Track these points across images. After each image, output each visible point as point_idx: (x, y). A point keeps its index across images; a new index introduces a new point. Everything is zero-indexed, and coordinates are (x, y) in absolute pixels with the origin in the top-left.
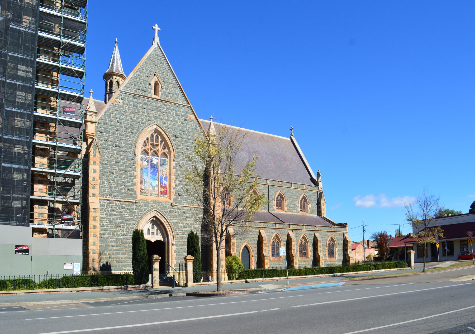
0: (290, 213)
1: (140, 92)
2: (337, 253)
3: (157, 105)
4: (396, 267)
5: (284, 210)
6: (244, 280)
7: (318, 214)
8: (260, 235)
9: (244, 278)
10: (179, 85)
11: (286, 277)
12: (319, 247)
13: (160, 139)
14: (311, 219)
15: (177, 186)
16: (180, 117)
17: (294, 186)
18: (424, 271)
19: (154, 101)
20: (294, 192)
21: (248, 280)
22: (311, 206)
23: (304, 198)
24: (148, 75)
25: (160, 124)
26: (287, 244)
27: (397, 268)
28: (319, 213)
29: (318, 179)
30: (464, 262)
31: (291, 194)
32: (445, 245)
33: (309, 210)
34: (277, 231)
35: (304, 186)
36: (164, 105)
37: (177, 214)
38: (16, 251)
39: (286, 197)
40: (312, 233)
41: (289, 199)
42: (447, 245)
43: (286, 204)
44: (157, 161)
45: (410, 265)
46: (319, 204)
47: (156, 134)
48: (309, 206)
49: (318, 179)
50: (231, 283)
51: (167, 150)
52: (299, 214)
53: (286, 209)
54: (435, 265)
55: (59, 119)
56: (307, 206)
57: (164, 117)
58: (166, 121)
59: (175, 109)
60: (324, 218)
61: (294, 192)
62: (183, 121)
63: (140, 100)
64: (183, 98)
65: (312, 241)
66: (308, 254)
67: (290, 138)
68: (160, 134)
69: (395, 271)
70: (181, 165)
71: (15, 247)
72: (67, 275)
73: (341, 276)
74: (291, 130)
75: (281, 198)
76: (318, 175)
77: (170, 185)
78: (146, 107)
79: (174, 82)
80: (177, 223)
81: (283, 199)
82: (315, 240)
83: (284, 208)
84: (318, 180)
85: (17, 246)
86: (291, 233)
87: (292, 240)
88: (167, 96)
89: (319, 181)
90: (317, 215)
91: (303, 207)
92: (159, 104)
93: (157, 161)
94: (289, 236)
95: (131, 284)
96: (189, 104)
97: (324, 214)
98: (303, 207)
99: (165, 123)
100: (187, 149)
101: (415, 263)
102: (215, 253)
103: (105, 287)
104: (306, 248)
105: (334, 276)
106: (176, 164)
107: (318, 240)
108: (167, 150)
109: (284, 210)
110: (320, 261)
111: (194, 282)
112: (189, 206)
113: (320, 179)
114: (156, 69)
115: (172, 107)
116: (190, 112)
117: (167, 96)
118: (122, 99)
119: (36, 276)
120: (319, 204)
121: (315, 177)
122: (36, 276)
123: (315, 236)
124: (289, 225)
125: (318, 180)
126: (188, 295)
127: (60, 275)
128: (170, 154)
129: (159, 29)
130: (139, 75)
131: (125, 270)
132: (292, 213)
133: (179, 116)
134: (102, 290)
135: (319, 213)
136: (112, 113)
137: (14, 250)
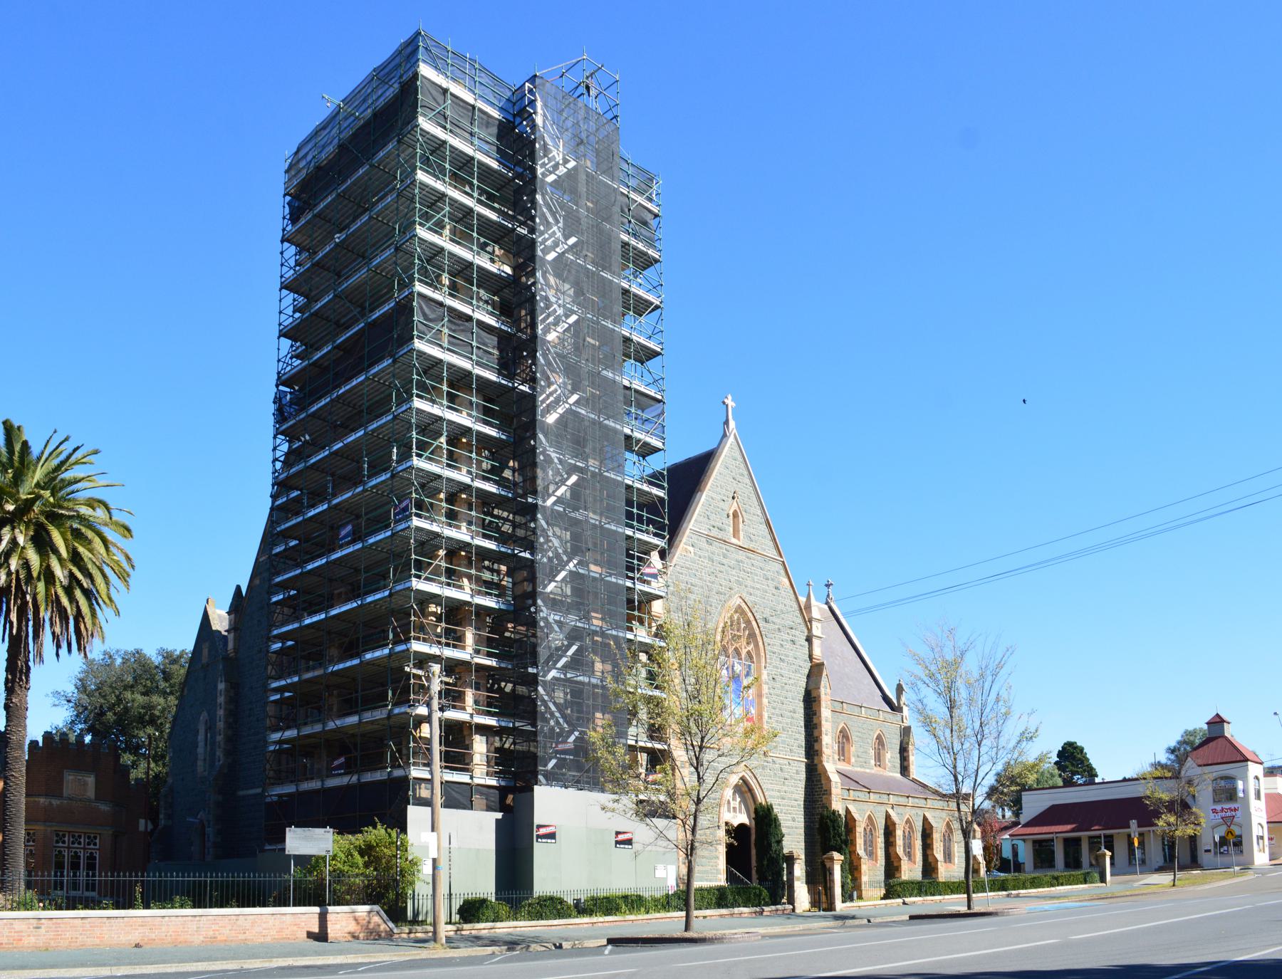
0: (859, 769)
1: (715, 533)
2: (956, 854)
3: (740, 558)
4: (1085, 882)
5: (849, 762)
6: (900, 901)
7: (901, 773)
8: (848, 816)
9: (899, 897)
10: (767, 519)
11: (985, 894)
12: (934, 841)
13: (743, 626)
14: (888, 782)
15: (771, 718)
16: (770, 581)
17: (866, 713)
18: (1174, 885)
19: (734, 549)
20: (865, 726)
21: (907, 900)
22: (891, 756)
23: (879, 737)
24: (724, 498)
25: (744, 595)
26: (885, 834)
27: (1086, 883)
28: (904, 770)
29: (899, 698)
30: (1217, 874)
31: (860, 730)
32: (1101, 842)
33: (889, 764)
34: (871, 806)
35: (881, 712)
36: (748, 558)
37: (772, 773)
38: (617, 842)
39: (854, 736)
40: (920, 812)
41: (857, 739)
42: (1105, 842)
43: (853, 749)
44: (740, 668)
45: (1103, 880)
46: (903, 751)
47: (738, 614)
48: (888, 756)
49: (899, 698)
50: (886, 905)
51: (752, 646)
52: (873, 772)
53: (853, 760)
54: (1142, 879)
55: (640, 591)
56: (884, 755)
57: (749, 583)
58: (751, 591)
59: (761, 565)
60: (914, 781)
61: (865, 726)
62: (774, 591)
63: (716, 548)
64: (771, 544)
65: (921, 829)
66: (914, 855)
67: (827, 603)
68: (743, 613)
69: (1084, 890)
70: (775, 677)
71: (614, 835)
72: (548, 894)
73: (1017, 896)
74: (828, 586)
75: (843, 736)
76: (900, 689)
77: (760, 716)
78: (724, 561)
79: (759, 512)
80: (772, 790)
81: (848, 739)
82: (889, 823)
83: (849, 759)
84: (899, 702)
85: (618, 833)
86: (891, 811)
87: (897, 826)
88: (752, 541)
89: (902, 703)
90: (899, 775)
91: (879, 758)
92: (741, 555)
93: (740, 668)
94: (890, 819)
95: (767, 905)
96: (781, 556)
97: (915, 772)
98: (879, 758)
99: (751, 594)
100: (782, 645)
101: (1111, 875)
102: (938, 845)
103: (736, 910)
104: (910, 843)
105: (1008, 896)
106: (768, 675)
107: (932, 827)
108: (752, 646)
109: (849, 762)
110: (937, 869)
111: (843, 902)
112: (787, 757)
113: (903, 699)
114: (735, 485)
115: (758, 561)
116: (782, 572)
117: (752, 541)
118: (693, 546)
119: (425, 897)
120: (903, 751)
121: (892, 695)
122: (425, 897)
123: (924, 816)
124: (889, 795)
125: (899, 702)
126: (912, 918)
127: (462, 896)
128: (758, 655)
129: (734, 405)
130: (712, 498)
131: (707, 880)
132: (862, 770)
133: (768, 579)
134: (732, 915)
135: (904, 770)
136: (682, 574)
137: (613, 840)
